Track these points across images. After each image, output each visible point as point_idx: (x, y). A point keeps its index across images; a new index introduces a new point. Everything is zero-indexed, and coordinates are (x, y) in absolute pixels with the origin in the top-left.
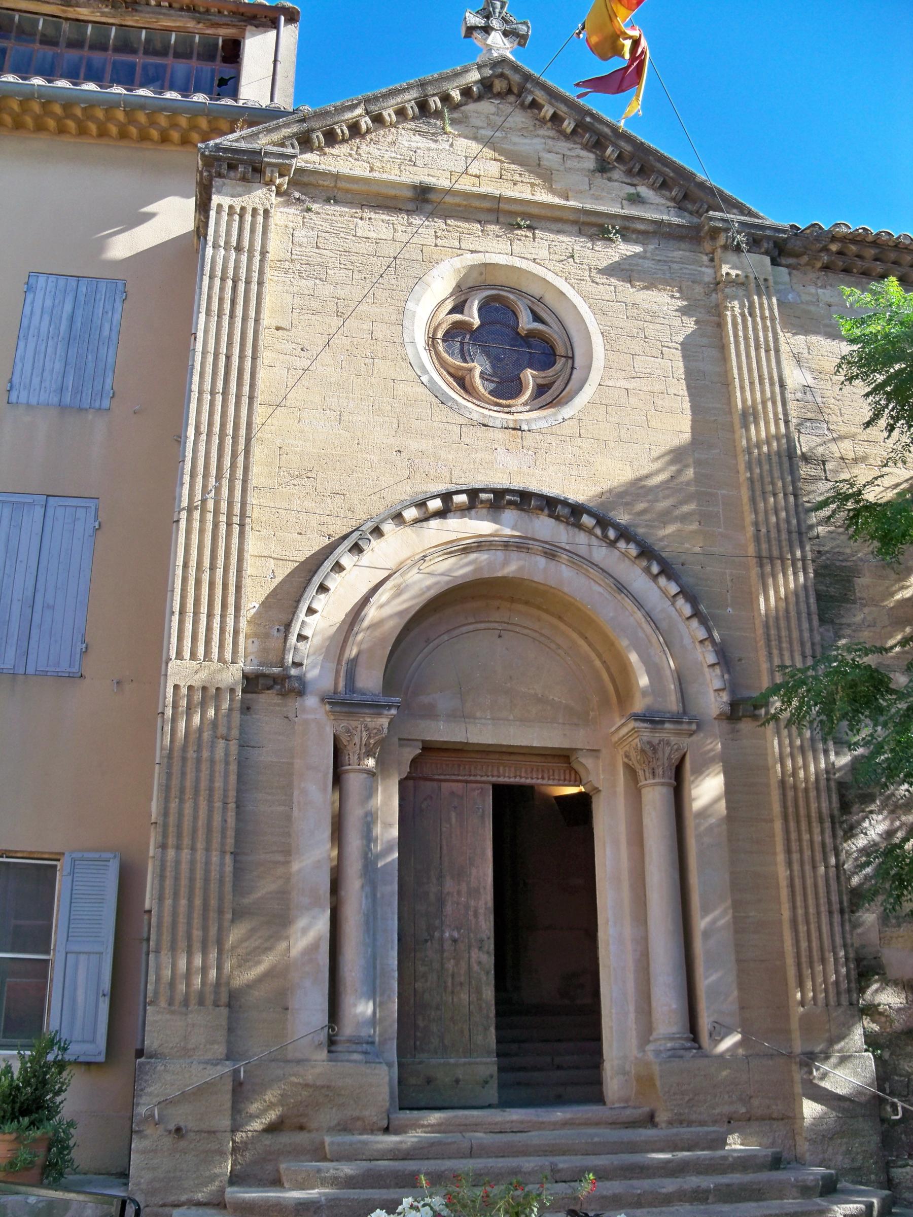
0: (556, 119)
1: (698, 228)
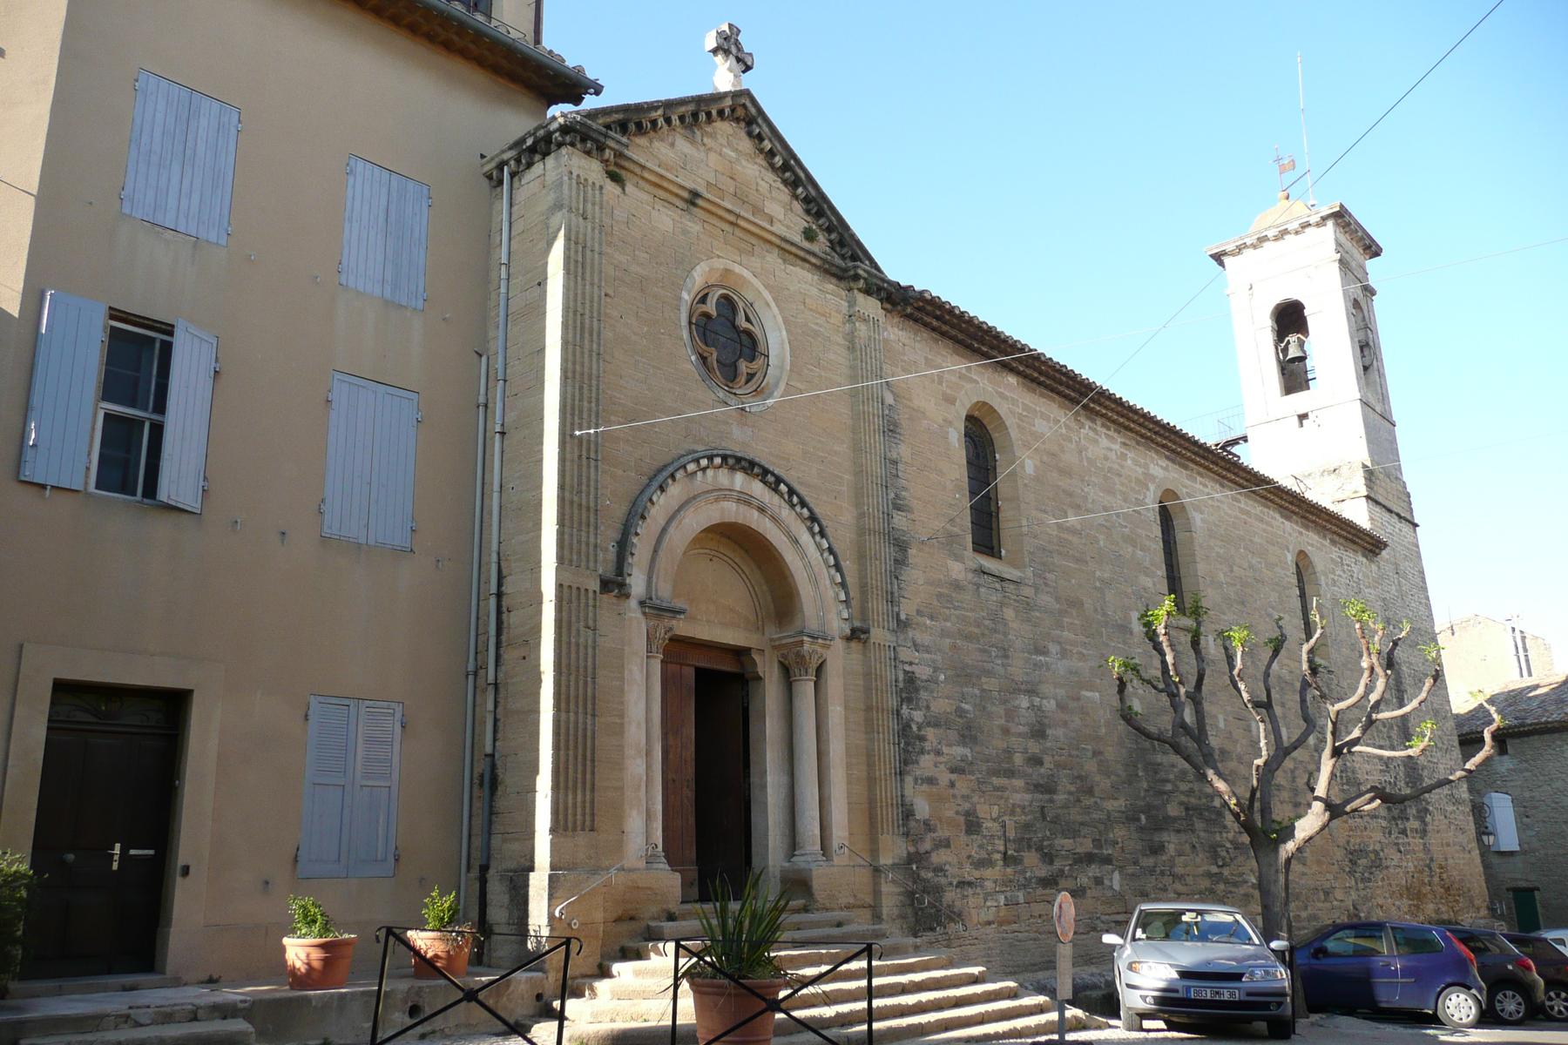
0: (771, 154)
1: (846, 270)
